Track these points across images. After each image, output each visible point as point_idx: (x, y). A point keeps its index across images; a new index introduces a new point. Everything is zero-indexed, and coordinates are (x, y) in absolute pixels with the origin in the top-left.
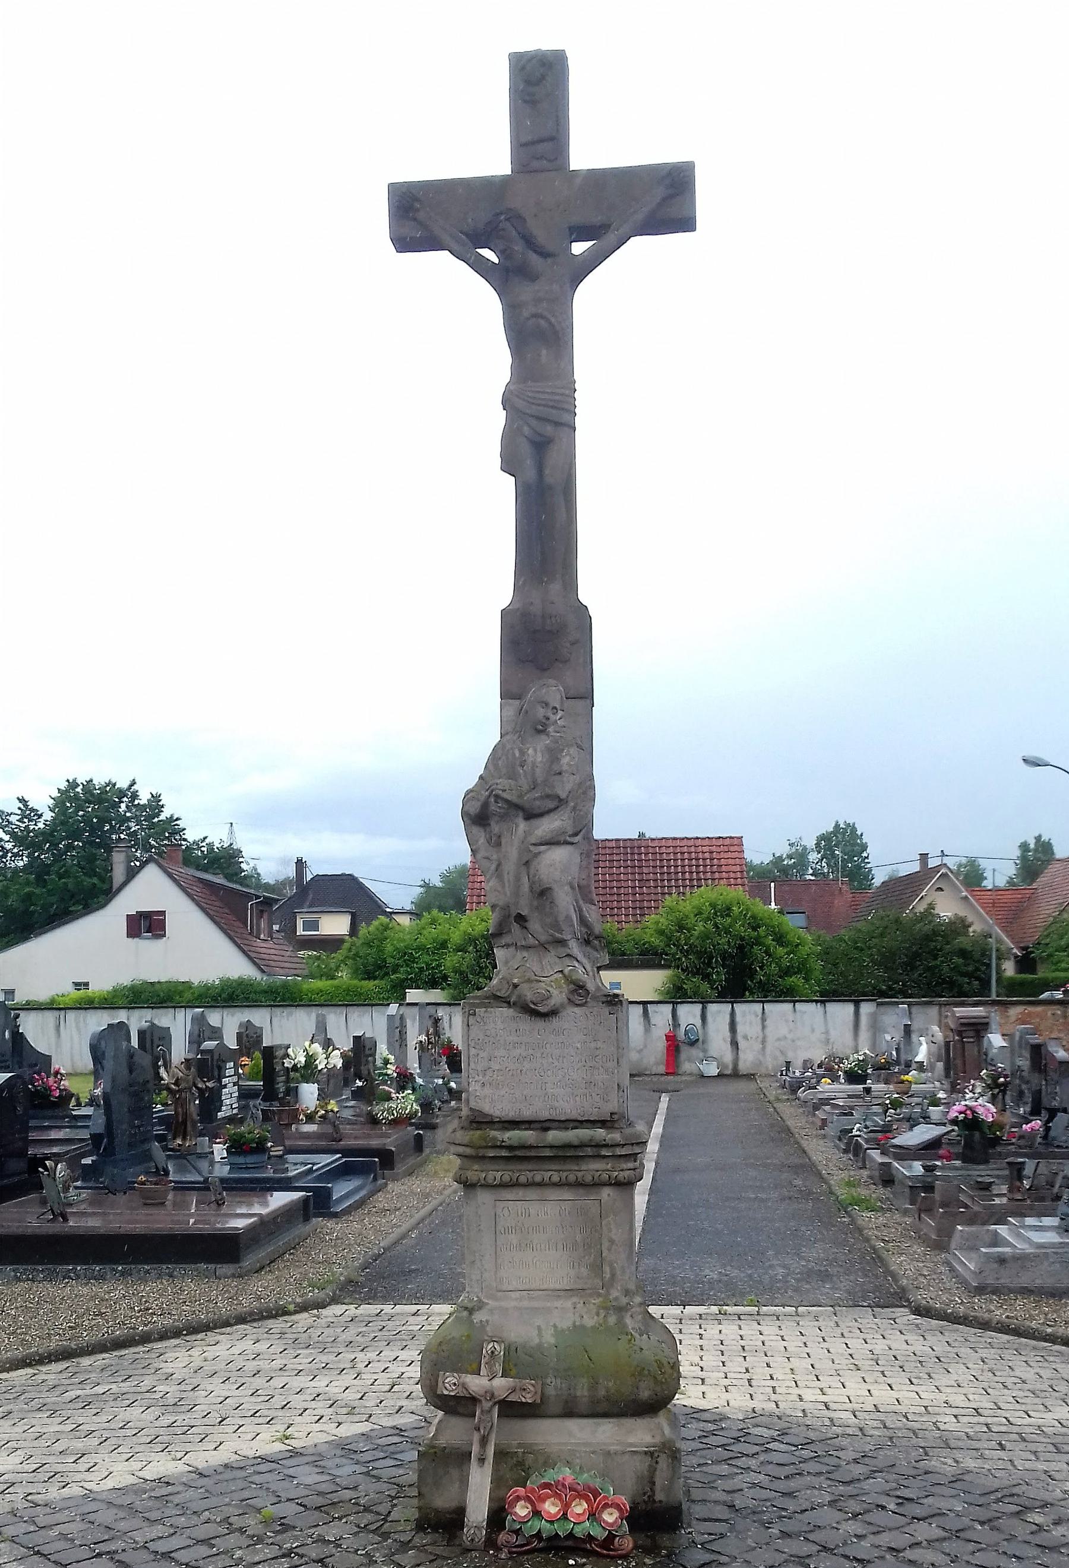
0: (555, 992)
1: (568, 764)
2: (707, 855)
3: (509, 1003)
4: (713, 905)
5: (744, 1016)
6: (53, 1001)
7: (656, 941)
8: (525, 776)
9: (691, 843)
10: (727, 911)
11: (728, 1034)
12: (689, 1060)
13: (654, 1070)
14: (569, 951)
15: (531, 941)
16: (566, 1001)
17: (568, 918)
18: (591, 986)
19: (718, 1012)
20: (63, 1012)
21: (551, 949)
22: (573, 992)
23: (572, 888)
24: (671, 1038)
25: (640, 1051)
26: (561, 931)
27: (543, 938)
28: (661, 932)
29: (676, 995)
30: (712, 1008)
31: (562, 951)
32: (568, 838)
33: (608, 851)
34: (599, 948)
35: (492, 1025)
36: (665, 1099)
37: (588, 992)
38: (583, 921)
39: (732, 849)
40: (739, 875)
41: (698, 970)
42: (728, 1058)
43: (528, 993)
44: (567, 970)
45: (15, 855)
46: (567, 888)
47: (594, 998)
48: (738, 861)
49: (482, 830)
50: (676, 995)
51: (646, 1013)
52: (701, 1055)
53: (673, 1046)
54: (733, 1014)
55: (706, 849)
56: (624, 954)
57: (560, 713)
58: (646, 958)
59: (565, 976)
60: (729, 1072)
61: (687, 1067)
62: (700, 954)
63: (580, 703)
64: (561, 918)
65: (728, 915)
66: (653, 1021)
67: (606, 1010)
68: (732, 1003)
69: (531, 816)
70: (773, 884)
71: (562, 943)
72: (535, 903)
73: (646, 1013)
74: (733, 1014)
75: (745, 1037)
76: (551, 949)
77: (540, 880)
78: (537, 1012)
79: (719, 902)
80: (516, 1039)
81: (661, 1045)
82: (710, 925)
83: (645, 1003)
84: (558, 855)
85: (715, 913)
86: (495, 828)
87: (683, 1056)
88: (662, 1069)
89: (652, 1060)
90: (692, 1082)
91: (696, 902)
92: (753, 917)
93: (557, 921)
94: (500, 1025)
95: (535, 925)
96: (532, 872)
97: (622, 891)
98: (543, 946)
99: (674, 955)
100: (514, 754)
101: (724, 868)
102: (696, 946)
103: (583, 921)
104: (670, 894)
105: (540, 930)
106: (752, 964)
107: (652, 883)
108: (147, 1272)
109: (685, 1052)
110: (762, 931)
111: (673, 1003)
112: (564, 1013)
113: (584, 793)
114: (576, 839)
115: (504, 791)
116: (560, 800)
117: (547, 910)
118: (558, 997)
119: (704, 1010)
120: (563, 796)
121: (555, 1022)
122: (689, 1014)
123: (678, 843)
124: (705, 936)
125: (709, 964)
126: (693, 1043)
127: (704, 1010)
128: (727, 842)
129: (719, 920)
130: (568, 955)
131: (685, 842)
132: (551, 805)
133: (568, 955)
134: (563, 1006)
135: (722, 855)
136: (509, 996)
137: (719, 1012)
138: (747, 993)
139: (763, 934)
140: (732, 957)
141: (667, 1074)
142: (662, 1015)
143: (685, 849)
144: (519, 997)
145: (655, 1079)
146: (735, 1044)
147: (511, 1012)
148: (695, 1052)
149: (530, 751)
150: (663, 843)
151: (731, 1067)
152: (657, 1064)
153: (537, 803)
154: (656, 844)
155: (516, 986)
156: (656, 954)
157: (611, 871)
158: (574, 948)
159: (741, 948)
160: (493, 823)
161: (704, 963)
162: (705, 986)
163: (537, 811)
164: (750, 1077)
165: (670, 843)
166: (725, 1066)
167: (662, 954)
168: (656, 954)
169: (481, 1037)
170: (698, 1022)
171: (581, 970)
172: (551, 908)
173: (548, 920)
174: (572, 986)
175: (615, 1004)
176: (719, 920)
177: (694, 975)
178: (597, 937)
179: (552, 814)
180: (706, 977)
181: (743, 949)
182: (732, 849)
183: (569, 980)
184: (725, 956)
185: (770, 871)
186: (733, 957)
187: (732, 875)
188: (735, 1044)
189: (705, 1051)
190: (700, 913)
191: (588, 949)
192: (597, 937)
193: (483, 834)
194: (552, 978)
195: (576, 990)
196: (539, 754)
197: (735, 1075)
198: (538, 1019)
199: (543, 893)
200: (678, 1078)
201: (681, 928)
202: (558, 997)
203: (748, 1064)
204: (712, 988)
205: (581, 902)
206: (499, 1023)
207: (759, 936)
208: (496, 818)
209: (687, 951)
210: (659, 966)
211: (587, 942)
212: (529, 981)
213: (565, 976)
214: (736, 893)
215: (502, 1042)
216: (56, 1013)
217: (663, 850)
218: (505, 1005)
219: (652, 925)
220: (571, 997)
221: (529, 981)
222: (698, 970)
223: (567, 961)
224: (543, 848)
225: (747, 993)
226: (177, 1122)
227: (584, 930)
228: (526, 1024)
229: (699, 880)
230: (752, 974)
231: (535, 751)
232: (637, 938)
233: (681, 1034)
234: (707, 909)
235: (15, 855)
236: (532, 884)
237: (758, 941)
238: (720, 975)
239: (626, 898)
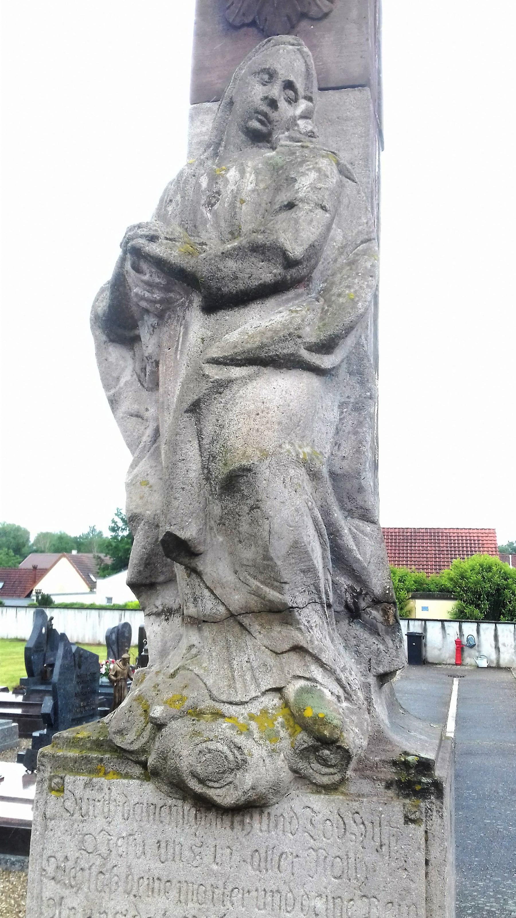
0: (256, 751)
1: (314, 188)
2: (476, 538)
3: (144, 765)
4: (481, 566)
5: (503, 631)
6: (126, 605)
7: (449, 584)
8: (217, 225)
9: (467, 531)
10: (489, 569)
11: (493, 643)
12: (470, 656)
13: (448, 662)
14: (301, 640)
15: (209, 606)
16: (286, 775)
17: (298, 549)
18: (355, 739)
19: (487, 628)
20: (123, 612)
21: (255, 628)
22: (305, 753)
23: (314, 476)
24: (459, 643)
25: (440, 650)
26: (277, 583)
27: (237, 599)
28: (451, 579)
29: (461, 617)
30: (483, 626)
31: (282, 636)
32: (305, 355)
33: (421, 534)
34: (381, 627)
35: (100, 822)
36: (456, 681)
37: (346, 756)
38: (340, 558)
39: (490, 535)
40: (494, 549)
41: (473, 601)
42: (493, 656)
43: (184, 750)
44: (292, 690)
45: (123, 529)
46: (299, 474)
47: (365, 769)
48: (493, 542)
49: (128, 355)
50: (461, 617)
51: (443, 627)
52: (477, 654)
53: (460, 647)
54: (496, 630)
55: (475, 535)
56: (430, 591)
57: (303, 105)
58: (444, 594)
59: (287, 704)
60: (494, 665)
61: (468, 660)
62: (475, 593)
63: (350, 97)
64: (279, 549)
65: (490, 571)
66: (447, 632)
67: (396, 808)
68: (496, 623)
69: (218, 301)
70: (510, 556)
71: (282, 614)
72: (216, 509)
73: (443, 627)
74: (496, 630)
75: (504, 645)
76: (255, 628)
77: (226, 450)
78: (205, 799)
79: (485, 564)
80: (157, 868)
81: (453, 647)
82: (479, 577)
83: (442, 621)
84: (278, 391)
85: (483, 570)
86: (149, 342)
87: (466, 654)
88: (453, 661)
89: (447, 655)
90: (472, 670)
91: (471, 563)
92: (505, 573)
93: (267, 557)
94: (119, 826)
95: (217, 566)
96: (209, 429)
97: (429, 556)
98: (235, 619)
99: (458, 593)
100: (198, 185)
101: (485, 546)
102: (471, 588)
103: (340, 558)
104: (456, 558)
105: (229, 577)
106: (504, 599)
107: (445, 552)
108: (13, 863)
109: (467, 651)
110: (510, 581)
111: (460, 622)
112: (280, 808)
113: (352, 263)
114: (326, 361)
115: (153, 239)
116: (290, 263)
117: (244, 527)
118: (265, 763)
119: (478, 627)
120: (296, 251)
121: (258, 826)
122: (469, 628)
123: (459, 531)
124: (477, 583)
125: (479, 599)
126: (472, 647)
127: (478, 627)
128: (487, 531)
129: (485, 573)
130: (297, 649)
131: (463, 531)
132: (266, 273)
133: (297, 649)
134: (277, 790)
135: (484, 538)
136: (144, 751)
137: (488, 628)
138: (502, 617)
139: (510, 583)
140: (493, 595)
141: (457, 664)
142: (453, 628)
143: (464, 534)
144: (164, 757)
145: (449, 667)
146: (497, 648)
147: (146, 792)
148: (473, 652)
149: (232, 174)
150: (451, 531)
151: (495, 662)
152: (450, 658)
153: (231, 265)
154: (447, 531)
155: (159, 726)
156: (448, 591)
157: (423, 545)
158: (317, 629)
159: (498, 590)
160: (144, 332)
161: (476, 598)
162: (477, 611)
163: (231, 288)
164: (508, 669)
165: (455, 531)
166: (492, 662)
167: (451, 592)
168: (448, 591)
169: (72, 853)
170: (475, 634)
171: (328, 688)
172: (254, 522)
173: (248, 554)
174: (303, 739)
175: (423, 794)
176: (485, 573)
177: (470, 604)
178: (376, 602)
179: (271, 302)
180: (478, 606)
181: (499, 590)
182: (490, 535)
183: (297, 720)
184: (488, 594)
185: (507, 550)
186: (493, 595)
187: (490, 549)
188: (497, 648)
189: (479, 652)
190: (474, 569)
191: (357, 630)
192: (376, 602)
193: (130, 361)
194: (254, 708)
195: (313, 749)
196: (250, 177)
197: (498, 667)
198: (211, 816)
199: (233, 484)
200: (463, 667)
201: (463, 577)
202: (265, 763)
203: (506, 661)
204: (481, 613)
205: (338, 514)
206: (118, 819)
207: (507, 585)
208: (152, 320)
209: (467, 591)
210: (450, 599)
211: (353, 613)
212: (197, 713)
213: (287, 704)
214: (496, 559)
215: (122, 870)
216: (120, 612)
217: (451, 534)
218: (137, 770)
219: (445, 576)
220: (302, 765)
221: (197, 713)
222: (473, 601)
223: (295, 664)
224: (236, 372)
225: (502, 617)
226: (115, 702)
227: (344, 581)
228: (183, 828)
229: (471, 551)
230: (504, 606)
231: (242, 172)
232: (437, 582)
233: (464, 641)
234: (478, 567)
235: (123, 529)
236: (209, 459)
237: (507, 587)
238: (486, 605)
239: (431, 560)
